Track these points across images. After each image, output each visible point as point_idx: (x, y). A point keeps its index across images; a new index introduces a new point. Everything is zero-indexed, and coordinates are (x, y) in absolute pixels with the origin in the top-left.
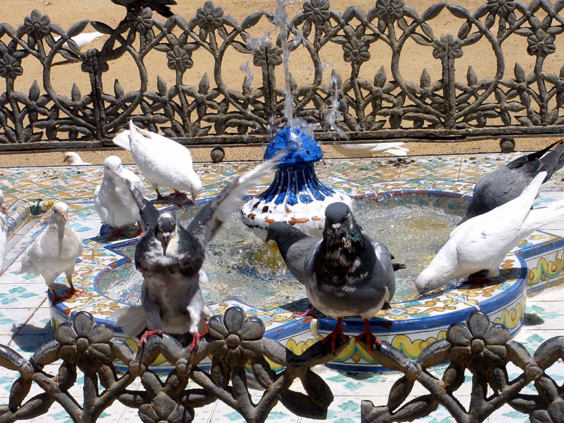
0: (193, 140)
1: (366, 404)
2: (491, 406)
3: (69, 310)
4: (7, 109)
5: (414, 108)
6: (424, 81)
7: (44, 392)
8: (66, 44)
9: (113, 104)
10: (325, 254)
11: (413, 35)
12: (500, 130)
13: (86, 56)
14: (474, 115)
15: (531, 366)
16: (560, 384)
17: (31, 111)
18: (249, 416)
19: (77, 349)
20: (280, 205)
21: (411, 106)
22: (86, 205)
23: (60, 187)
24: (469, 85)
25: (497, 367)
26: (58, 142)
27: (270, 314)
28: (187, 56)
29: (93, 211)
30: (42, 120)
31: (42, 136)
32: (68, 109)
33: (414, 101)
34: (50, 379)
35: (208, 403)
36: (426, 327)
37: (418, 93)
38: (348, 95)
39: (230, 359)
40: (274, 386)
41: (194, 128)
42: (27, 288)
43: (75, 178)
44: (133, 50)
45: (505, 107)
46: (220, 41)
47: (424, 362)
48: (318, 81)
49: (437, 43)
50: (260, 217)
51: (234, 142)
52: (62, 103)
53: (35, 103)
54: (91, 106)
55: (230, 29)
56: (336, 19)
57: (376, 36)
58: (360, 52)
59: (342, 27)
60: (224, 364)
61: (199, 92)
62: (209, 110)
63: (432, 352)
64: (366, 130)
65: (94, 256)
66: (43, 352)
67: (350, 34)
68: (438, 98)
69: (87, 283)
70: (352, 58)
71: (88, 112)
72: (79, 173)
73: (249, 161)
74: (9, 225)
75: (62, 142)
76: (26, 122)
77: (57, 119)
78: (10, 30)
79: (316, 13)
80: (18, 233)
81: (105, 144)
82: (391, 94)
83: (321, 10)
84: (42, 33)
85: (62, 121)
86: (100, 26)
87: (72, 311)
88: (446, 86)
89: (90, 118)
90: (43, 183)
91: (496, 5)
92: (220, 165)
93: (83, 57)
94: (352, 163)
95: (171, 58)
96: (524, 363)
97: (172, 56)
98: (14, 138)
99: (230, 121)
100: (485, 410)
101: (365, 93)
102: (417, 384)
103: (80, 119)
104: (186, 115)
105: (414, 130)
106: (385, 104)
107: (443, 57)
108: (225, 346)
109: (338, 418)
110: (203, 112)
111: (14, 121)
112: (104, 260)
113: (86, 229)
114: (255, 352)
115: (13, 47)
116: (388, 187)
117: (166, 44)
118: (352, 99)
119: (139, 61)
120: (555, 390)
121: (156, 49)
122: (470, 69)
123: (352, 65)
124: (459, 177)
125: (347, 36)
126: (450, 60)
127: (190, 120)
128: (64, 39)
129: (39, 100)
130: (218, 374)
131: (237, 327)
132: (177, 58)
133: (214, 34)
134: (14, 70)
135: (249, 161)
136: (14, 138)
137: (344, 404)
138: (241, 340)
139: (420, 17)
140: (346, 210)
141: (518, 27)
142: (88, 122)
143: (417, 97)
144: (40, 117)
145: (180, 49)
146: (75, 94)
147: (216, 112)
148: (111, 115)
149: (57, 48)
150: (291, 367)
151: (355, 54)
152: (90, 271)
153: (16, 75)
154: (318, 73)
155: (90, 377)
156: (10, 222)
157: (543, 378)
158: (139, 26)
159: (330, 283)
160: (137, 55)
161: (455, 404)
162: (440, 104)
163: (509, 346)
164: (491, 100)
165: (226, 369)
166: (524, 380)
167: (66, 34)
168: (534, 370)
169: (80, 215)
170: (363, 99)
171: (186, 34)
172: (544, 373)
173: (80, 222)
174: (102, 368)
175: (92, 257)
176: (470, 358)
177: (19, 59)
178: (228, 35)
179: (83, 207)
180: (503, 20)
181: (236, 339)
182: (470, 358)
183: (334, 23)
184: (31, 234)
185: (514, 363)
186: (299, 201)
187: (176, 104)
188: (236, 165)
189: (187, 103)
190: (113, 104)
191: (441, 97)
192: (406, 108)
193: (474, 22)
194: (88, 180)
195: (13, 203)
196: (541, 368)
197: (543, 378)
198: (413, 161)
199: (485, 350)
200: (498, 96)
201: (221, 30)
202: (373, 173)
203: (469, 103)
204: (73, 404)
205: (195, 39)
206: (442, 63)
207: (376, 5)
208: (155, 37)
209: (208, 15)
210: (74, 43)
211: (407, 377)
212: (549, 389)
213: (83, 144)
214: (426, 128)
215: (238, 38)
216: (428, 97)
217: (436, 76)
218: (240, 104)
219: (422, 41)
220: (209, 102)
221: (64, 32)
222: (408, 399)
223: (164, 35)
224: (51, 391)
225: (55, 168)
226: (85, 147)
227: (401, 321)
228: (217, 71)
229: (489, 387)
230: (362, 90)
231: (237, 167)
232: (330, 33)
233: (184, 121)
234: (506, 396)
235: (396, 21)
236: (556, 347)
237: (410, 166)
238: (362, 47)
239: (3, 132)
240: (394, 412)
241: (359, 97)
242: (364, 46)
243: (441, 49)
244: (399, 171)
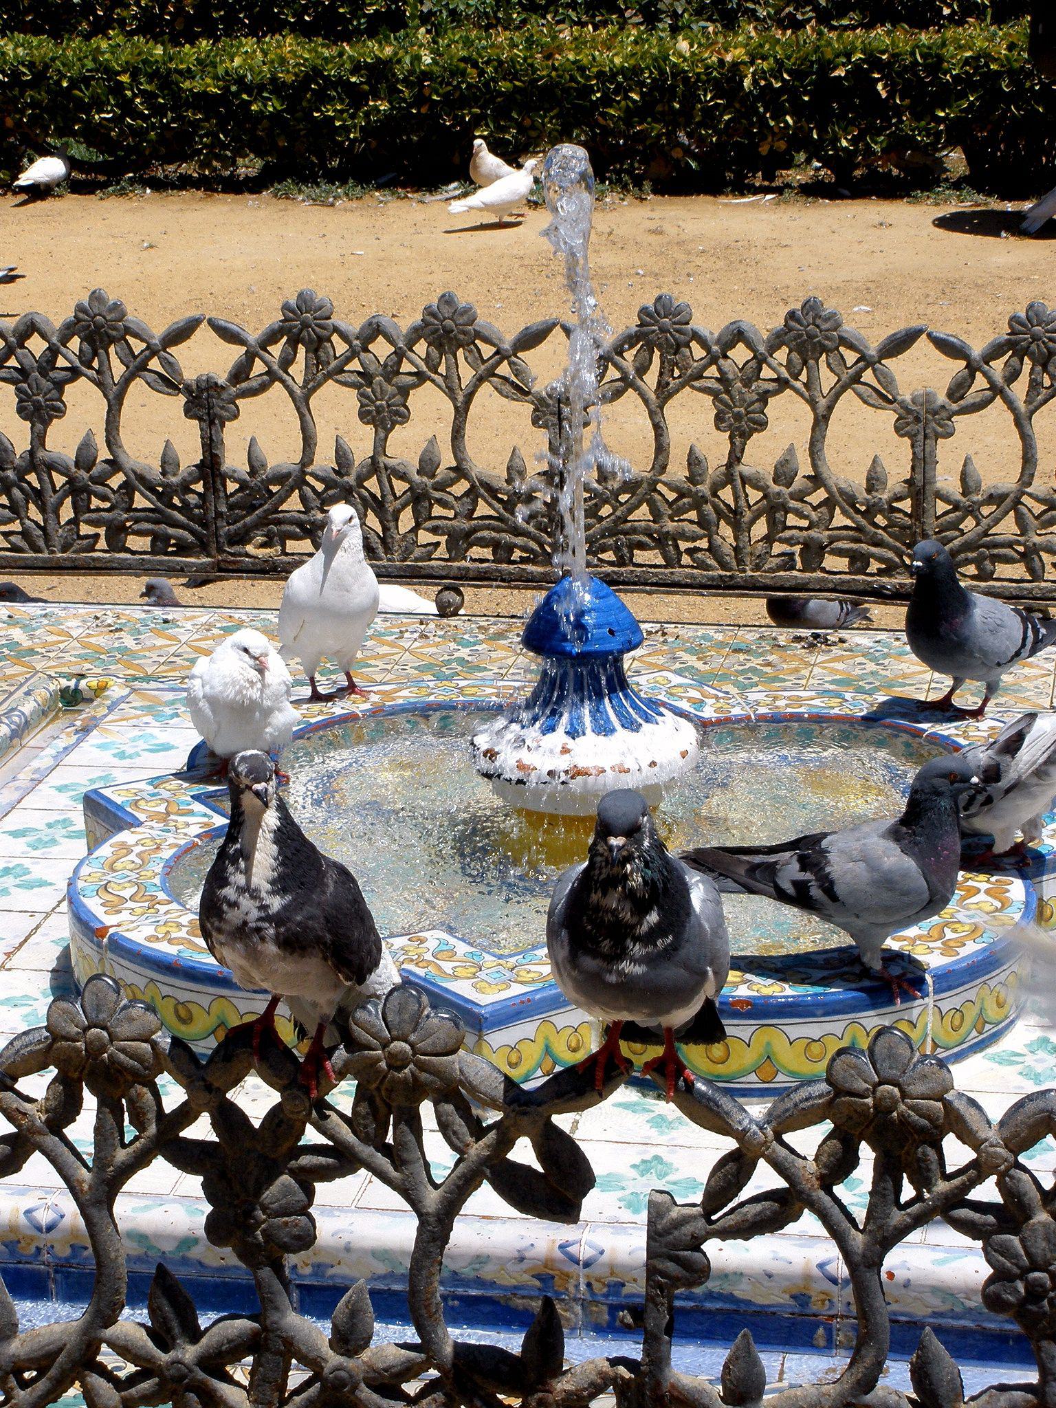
0: (401, 568)
1: (659, 1198)
2: (909, 1220)
3: (107, 928)
4: (29, 484)
5: (851, 533)
6: (874, 481)
7: (16, 1130)
8: (154, 364)
9: (243, 486)
10: (589, 896)
11: (855, 386)
12: (1021, 589)
13: (194, 387)
14: (971, 555)
15: (992, 1146)
16: (1048, 1185)
17: (76, 490)
18: (424, 1207)
19: (86, 1050)
20: (550, 736)
21: (846, 528)
22: (170, 696)
23: (125, 650)
24: (964, 494)
25: (924, 1143)
26: (129, 556)
27: (510, 965)
28: (398, 399)
29: (183, 709)
30: (98, 510)
31: (96, 542)
32: (152, 490)
33: (852, 519)
34: (28, 1106)
35: (343, 1175)
36: (820, 1012)
37: (862, 504)
38: (719, 497)
39: (390, 1091)
40: (478, 1149)
41: (404, 544)
42: (33, 868)
43: (158, 633)
44: (290, 382)
45: (1034, 544)
46: (467, 374)
47: (779, 1124)
48: (660, 464)
49: (903, 405)
50: (508, 760)
51: (482, 578)
52: (141, 478)
53: (86, 475)
54: (199, 487)
55: (487, 351)
56: (704, 344)
57: (782, 384)
58: (748, 413)
59: (713, 360)
60: (378, 1100)
61: (418, 472)
62: (437, 511)
63: (796, 1105)
64: (752, 570)
65: (168, 814)
66: (18, 1051)
67: (731, 376)
68: (901, 515)
69: (149, 874)
70: (731, 425)
71: (192, 499)
72: (166, 621)
73: (513, 617)
74: (13, 727)
75: (138, 557)
76: (67, 512)
77: (129, 509)
78: (43, 326)
79: (663, 330)
80: (32, 743)
81: (223, 565)
82: (805, 502)
83: (675, 323)
84: (108, 336)
85: (138, 514)
87: (111, 931)
88: (918, 493)
89: (196, 511)
90: (92, 640)
91: (1025, 339)
92: (453, 621)
93: (188, 390)
94: (719, 637)
95: (365, 401)
96: (977, 1139)
97: (367, 397)
98: (41, 543)
99: (479, 534)
100: (895, 1228)
101: (754, 495)
102: (762, 1166)
103: (175, 513)
104: (390, 518)
105: (848, 577)
106: (792, 520)
107: (915, 435)
108: (383, 1064)
109: (627, 1192)
110: (424, 514)
111: (43, 510)
112: (188, 825)
113: (166, 747)
114: (441, 1079)
115: (48, 362)
116: (778, 703)
117: (359, 373)
118: (728, 506)
119: (302, 404)
120: (1038, 1196)
121: (337, 381)
122: (253, 443)
123: (731, 438)
124: (932, 681)
125: (723, 379)
126: (928, 441)
127: (397, 528)
128: (152, 351)
129: (95, 471)
130: (364, 1118)
131: (408, 1027)
132: (378, 403)
133: (456, 359)
134: (47, 406)
135: (513, 617)
136: (41, 543)
137: (643, 1161)
138: (414, 1055)
139: (872, 350)
140: (639, 807)
142: (192, 520)
143: (858, 511)
144: (95, 503)
145: (385, 384)
146: (168, 462)
147: (451, 514)
148: (240, 508)
149: (137, 368)
150: (512, 1115)
151: (738, 417)
152: (158, 848)
153: (51, 418)
154: (661, 449)
155: (110, 1107)
156: (16, 719)
157: (1013, 1172)
158: (305, 333)
159: (596, 954)
160: (298, 391)
161: (836, 1210)
162: (904, 528)
163: (950, 1102)
164: (1007, 527)
165: (383, 1109)
166: (976, 1171)
167: (156, 341)
168: (996, 1156)
169: (157, 716)
170: (749, 507)
171: (399, 355)
172: (1016, 1160)
173: (156, 732)
174: (132, 1091)
175: (165, 817)
176: (872, 1121)
177: (60, 386)
178: (484, 362)
179: (164, 699)
180: (1039, 368)
181: (403, 1052)
182: (872, 1121)
183: (698, 352)
184: (54, 752)
185: (959, 1137)
186: (589, 731)
187: (370, 493)
188: (485, 624)
189: (394, 494)
190: (243, 486)
191: (905, 514)
192: (835, 532)
193: (979, 369)
194: (184, 639)
195: (27, 680)
196: (1011, 1151)
197: (1013, 1172)
198: (842, 641)
199: (902, 1107)
200: (1020, 520)
201: (471, 351)
202: (760, 661)
203: (961, 530)
204: (73, 1158)
205: (416, 366)
206: (913, 446)
207: (786, 321)
208: (336, 358)
209: (445, 319)
210: (171, 359)
211: (744, 1151)
212: (1025, 1194)
213: (178, 563)
214: (872, 575)
215: (504, 369)
216: (881, 511)
218: (500, 501)
219: (875, 399)
220: (437, 495)
221: (153, 337)
222: (747, 1193)
223: (353, 354)
224: (28, 1130)
225: (119, 609)
226: (182, 570)
227: (772, 997)
228: (457, 434)
229: (905, 1181)
230: (748, 489)
231: (486, 629)
232: (690, 371)
233: (385, 529)
234: (939, 1204)
235: (824, 355)
236: (1042, 1111)
237: (836, 651)
238: (753, 403)
239: (20, 529)
240: (714, 1217)
241: (742, 502)
242: (757, 400)
243: (911, 418)
244: (812, 659)
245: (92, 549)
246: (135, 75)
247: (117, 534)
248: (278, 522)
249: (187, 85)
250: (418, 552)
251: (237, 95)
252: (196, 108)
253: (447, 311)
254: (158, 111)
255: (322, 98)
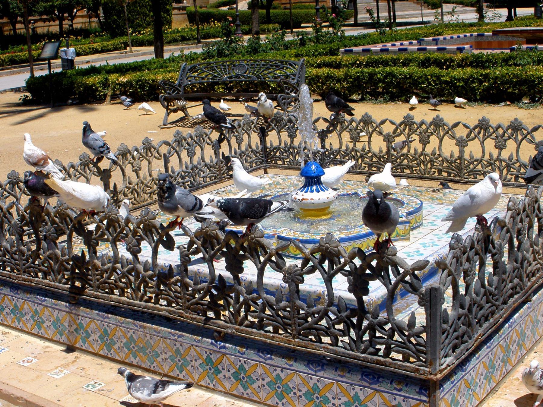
48: (280, 144)
49: (457, 139)
78: (502, 126)
86: (325, 120)
101: (504, 164)
119: (482, 143)
141: (491, 135)
151: (423, 141)
154: (483, 152)
162: (458, 166)
164: (479, 167)
171: (504, 133)
217: (456, 154)
219: (451, 137)
223: (494, 132)
245: (364, 169)
246: (431, 76)
247: (440, 172)
248: (335, 161)
249: (443, 79)
250: (431, 173)
251: (454, 81)
252: (445, 84)
253: (366, 116)
254: (437, 84)
255: (473, 82)
